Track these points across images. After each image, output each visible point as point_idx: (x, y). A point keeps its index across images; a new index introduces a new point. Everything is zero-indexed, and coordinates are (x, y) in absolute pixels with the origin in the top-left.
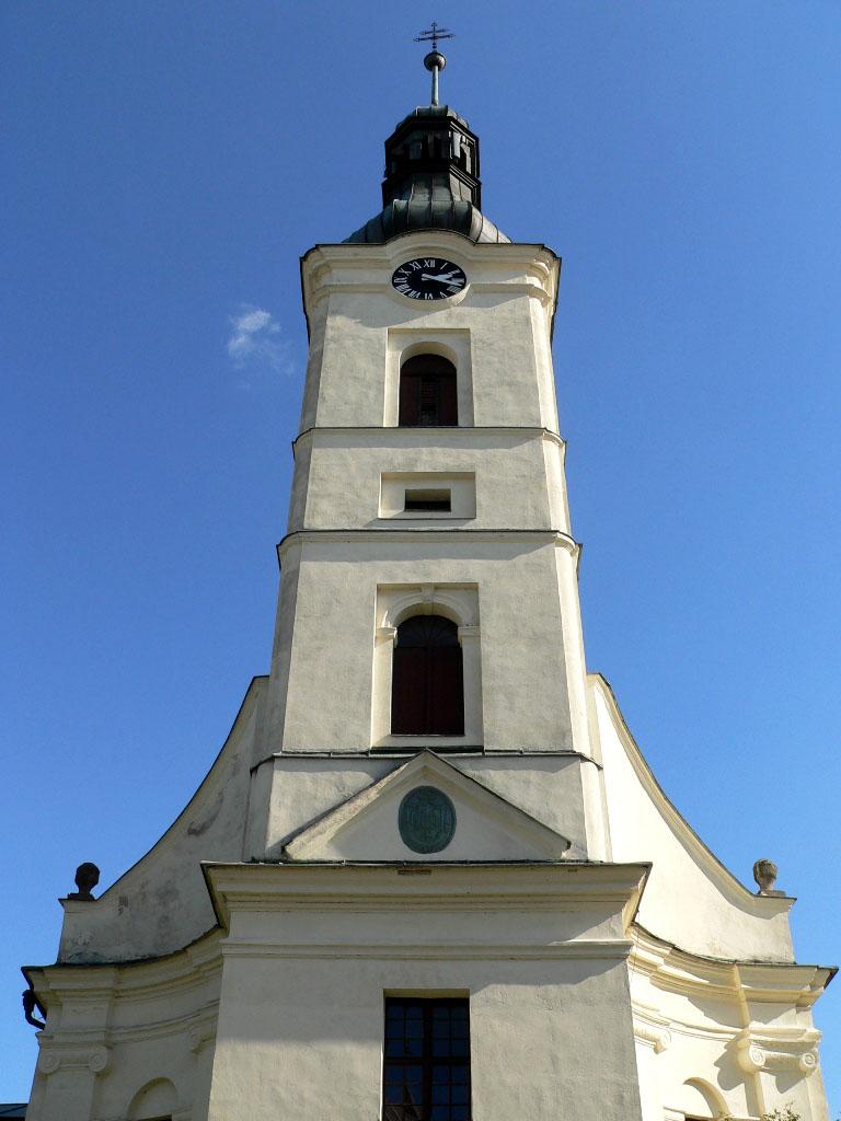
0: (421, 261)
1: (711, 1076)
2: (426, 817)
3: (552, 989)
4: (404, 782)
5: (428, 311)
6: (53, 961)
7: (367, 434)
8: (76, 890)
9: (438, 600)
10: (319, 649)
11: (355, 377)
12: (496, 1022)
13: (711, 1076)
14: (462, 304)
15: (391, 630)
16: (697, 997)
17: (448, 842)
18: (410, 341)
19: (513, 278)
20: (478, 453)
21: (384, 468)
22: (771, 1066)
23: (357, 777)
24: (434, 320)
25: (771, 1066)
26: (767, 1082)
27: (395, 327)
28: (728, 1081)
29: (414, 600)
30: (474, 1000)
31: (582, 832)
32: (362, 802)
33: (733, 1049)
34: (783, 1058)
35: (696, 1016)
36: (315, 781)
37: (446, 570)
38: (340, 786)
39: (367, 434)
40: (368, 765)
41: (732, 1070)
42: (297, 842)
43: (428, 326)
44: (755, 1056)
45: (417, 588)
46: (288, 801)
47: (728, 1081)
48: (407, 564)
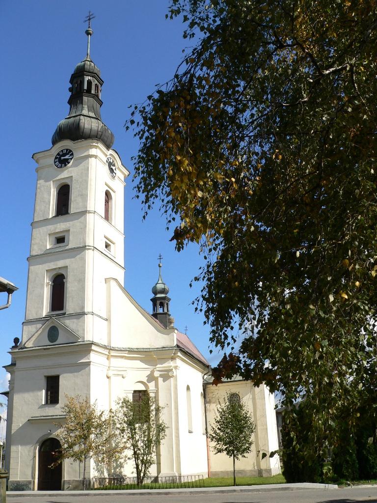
0: (62, 151)
1: (145, 380)
2: (53, 333)
3: (75, 374)
4: (49, 325)
5: (63, 171)
6: (10, 363)
7: (46, 221)
8: (14, 345)
9: (60, 272)
10: (33, 291)
11: (44, 201)
12: (64, 381)
13: (145, 380)
14: (71, 167)
15: (49, 283)
16: (142, 360)
17: (57, 339)
18: (59, 183)
19: (85, 152)
20: (71, 223)
21: (49, 232)
22: (161, 376)
23: (39, 326)
24: (64, 174)
25: (161, 376)
26: (160, 380)
27: (55, 179)
28: (149, 381)
29: (55, 273)
30: (60, 377)
31: (84, 334)
32: (39, 332)
33: (152, 372)
34: (164, 374)
35: (143, 365)
36: (32, 327)
37: (60, 263)
38: (36, 328)
39: (46, 221)
40: (41, 322)
41: (151, 378)
42: (26, 344)
43: (63, 177)
44: (157, 374)
45: (55, 269)
46: (26, 333)
47: (149, 381)
48: (52, 263)
